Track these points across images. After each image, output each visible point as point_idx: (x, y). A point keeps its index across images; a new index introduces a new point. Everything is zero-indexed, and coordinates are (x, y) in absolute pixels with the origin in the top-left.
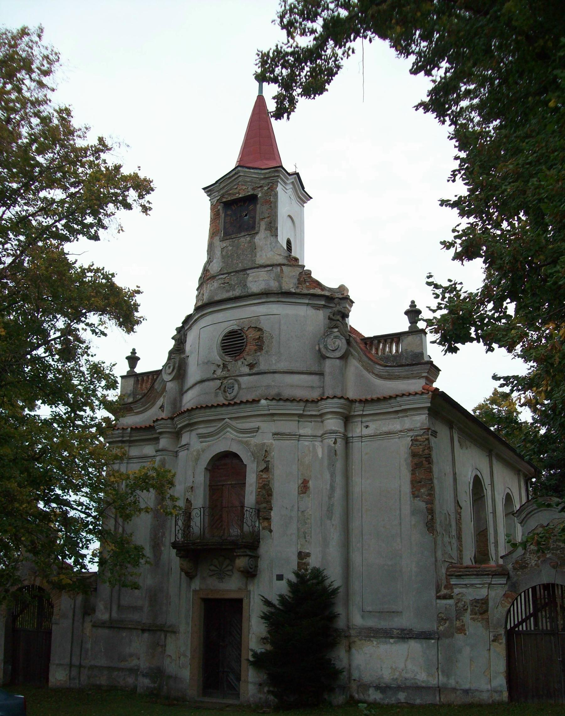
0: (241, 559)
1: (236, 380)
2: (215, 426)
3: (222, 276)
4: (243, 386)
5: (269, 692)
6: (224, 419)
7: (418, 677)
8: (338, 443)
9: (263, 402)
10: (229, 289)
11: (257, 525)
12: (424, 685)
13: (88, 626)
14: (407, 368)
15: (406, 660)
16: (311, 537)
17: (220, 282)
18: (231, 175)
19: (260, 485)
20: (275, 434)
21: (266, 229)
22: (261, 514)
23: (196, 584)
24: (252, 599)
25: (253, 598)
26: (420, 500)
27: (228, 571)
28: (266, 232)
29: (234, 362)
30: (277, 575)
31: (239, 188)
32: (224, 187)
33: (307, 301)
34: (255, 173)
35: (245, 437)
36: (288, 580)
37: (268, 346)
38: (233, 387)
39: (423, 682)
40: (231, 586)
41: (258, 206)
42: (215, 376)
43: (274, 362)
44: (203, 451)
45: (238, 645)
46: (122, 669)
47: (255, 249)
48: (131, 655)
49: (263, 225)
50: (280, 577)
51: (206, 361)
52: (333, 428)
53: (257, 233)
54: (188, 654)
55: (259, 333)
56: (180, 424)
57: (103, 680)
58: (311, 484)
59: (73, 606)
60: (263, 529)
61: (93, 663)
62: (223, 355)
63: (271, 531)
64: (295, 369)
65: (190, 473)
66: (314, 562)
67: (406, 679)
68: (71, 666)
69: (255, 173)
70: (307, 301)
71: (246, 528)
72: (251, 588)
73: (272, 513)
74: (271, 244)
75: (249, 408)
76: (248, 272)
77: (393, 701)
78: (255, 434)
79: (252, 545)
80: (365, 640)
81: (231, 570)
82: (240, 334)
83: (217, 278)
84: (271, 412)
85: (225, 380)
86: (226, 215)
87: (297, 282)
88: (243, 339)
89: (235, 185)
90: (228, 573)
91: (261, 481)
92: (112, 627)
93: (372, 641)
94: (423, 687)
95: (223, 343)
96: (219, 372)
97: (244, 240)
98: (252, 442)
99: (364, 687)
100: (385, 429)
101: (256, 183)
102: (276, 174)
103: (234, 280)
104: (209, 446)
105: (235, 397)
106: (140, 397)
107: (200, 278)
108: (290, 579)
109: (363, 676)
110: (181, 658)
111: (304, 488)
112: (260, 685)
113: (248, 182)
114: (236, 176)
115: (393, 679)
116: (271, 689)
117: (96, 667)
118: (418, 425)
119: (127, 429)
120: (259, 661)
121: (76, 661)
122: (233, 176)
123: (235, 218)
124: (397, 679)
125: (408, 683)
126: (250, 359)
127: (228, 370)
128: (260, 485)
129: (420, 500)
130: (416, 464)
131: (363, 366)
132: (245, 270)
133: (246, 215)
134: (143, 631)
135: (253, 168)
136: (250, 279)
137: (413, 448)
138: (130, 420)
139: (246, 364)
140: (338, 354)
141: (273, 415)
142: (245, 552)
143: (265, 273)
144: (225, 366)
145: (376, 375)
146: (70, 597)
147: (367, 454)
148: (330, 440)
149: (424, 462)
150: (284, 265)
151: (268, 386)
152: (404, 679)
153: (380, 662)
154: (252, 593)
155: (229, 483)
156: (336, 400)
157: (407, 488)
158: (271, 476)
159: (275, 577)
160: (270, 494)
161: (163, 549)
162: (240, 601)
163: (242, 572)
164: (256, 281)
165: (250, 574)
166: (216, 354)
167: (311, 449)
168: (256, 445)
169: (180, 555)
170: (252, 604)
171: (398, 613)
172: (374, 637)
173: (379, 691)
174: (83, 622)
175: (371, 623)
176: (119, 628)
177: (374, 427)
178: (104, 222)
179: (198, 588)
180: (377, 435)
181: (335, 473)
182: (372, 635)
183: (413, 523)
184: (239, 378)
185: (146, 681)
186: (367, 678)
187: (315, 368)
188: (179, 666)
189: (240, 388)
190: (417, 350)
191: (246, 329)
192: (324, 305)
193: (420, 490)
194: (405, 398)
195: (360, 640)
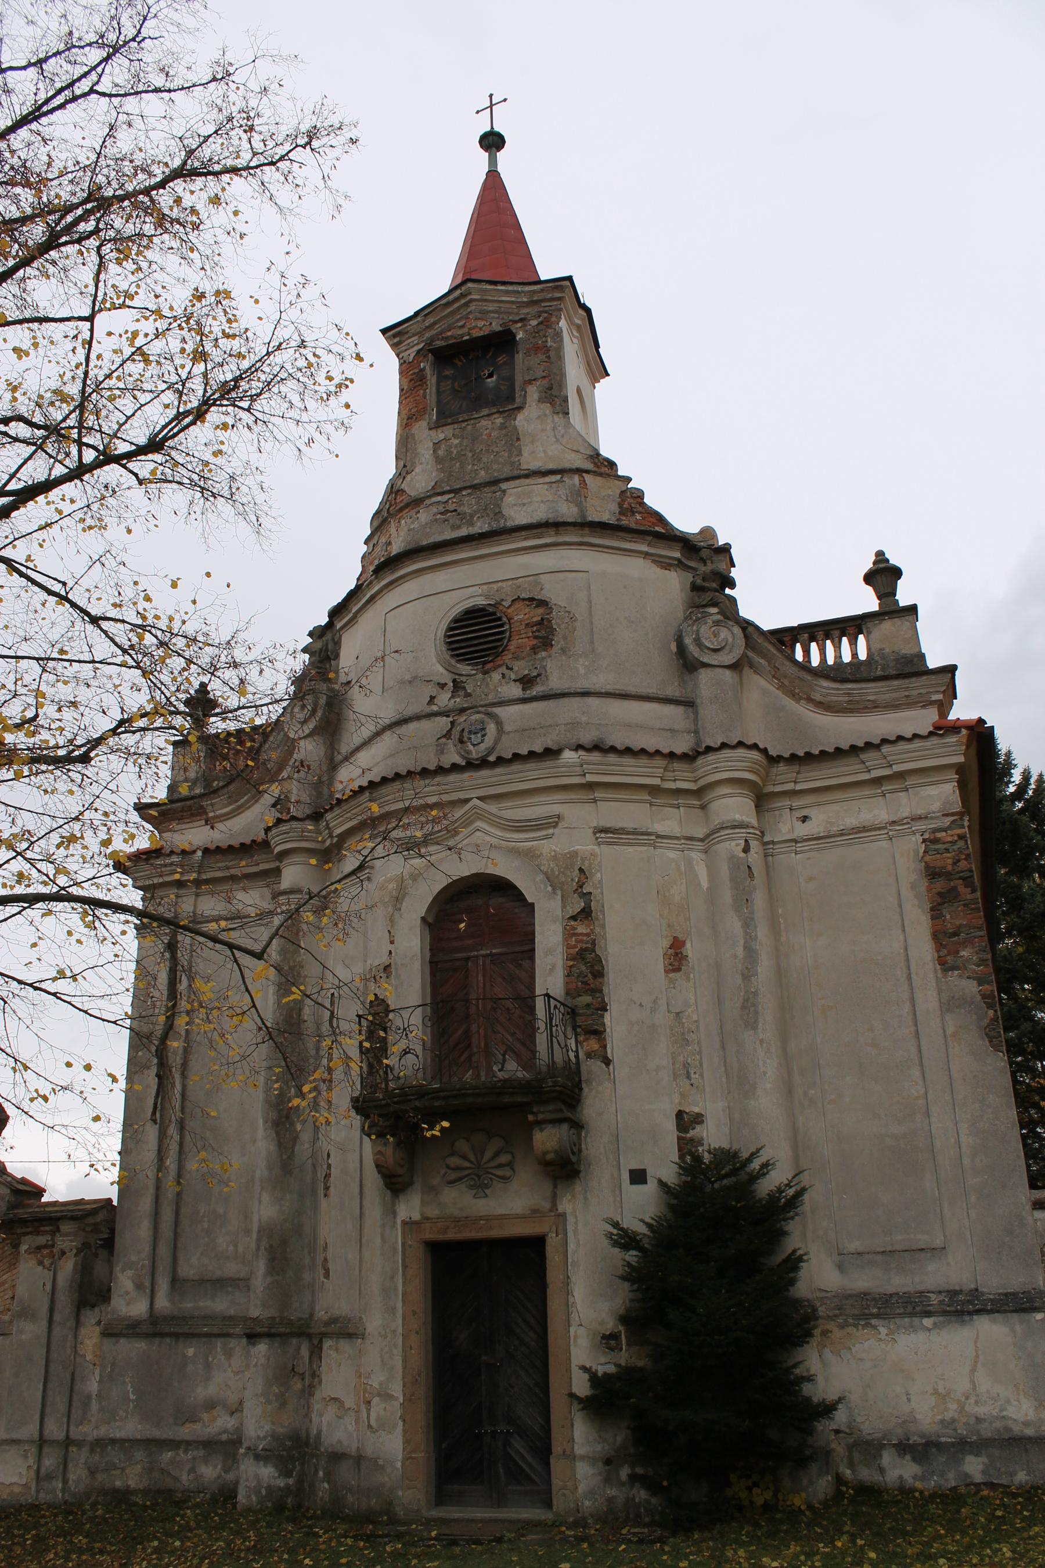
0: (546, 1133)
1: (489, 714)
3: (439, 498)
4: (508, 728)
5: (633, 1478)
6: (467, 801)
7: (1011, 1412)
8: (752, 851)
9: (568, 755)
10: (458, 522)
12: (1029, 1432)
13: (90, 1337)
14: (896, 683)
15: (973, 1371)
16: (702, 1075)
17: (435, 510)
18: (451, 298)
19: (571, 951)
20: (601, 831)
21: (540, 400)
22: (580, 1021)
23: (410, 1208)
24: (570, 1234)
25: (576, 1230)
26: (960, 976)
27: (500, 1166)
28: (542, 406)
29: (480, 676)
30: (631, 1172)
31: (468, 325)
32: (435, 323)
33: (645, 548)
34: (507, 292)
35: (523, 840)
36: (660, 1181)
37: (565, 638)
38: (483, 729)
39: (1026, 1424)
40: (509, 1205)
41: (519, 357)
42: (435, 708)
43: (582, 671)
44: (414, 877)
45: (539, 1358)
46: (188, 1444)
47: (518, 439)
48: (211, 1405)
49: (533, 393)
50: (638, 1177)
51: (408, 677)
52: (738, 817)
53: (520, 408)
54: (397, 1390)
55: (540, 611)
56: (341, 824)
57: (132, 1477)
58: (689, 949)
59: (49, 1287)
60: (589, 1056)
61: (103, 1432)
62: (453, 662)
63: (607, 1062)
64: (632, 690)
66: (713, 1135)
67: (979, 1420)
68: (42, 1442)
69: (507, 292)
70: (645, 548)
72: (565, 1205)
73: (607, 1019)
74: (554, 429)
75: (532, 775)
76: (504, 486)
77: (951, 1480)
78: (551, 831)
79: (561, 1095)
80: (856, 1326)
82: (494, 614)
83: (428, 502)
84: (589, 778)
85: (462, 716)
86: (441, 379)
87: (617, 510)
88: (502, 626)
89: (458, 321)
90: (500, 1172)
91: (573, 941)
92: (154, 1335)
93: (875, 1327)
94: (1029, 1439)
95: (450, 636)
96: (444, 699)
97: (489, 425)
98: (545, 851)
99: (868, 1448)
100: (851, 821)
101: (510, 313)
102: (557, 295)
103: (469, 503)
105: (491, 751)
106: (221, 784)
107: (378, 513)
108: (664, 1180)
109: (859, 1419)
110: (371, 1403)
111: (676, 957)
112: (608, 1462)
113: (491, 312)
114: (463, 301)
115: (942, 1421)
116: (639, 1470)
117: (113, 1441)
118: (936, 806)
119: (194, 852)
120: (605, 1399)
121: (54, 1430)
122: (457, 300)
123: (463, 383)
124: (953, 1421)
125: (986, 1431)
126: (522, 668)
128: (571, 951)
129: (960, 976)
130: (939, 894)
131: (781, 687)
132: (496, 482)
133: (491, 376)
134: (252, 1337)
135: (504, 283)
136: (509, 500)
137: (927, 858)
138: (194, 836)
139: (513, 677)
140: (728, 659)
141: (591, 786)
142: (561, 1110)
143: (546, 486)
144: (458, 686)
145: (819, 704)
146: (41, 1263)
147: (811, 879)
148: (733, 843)
149: (961, 889)
150: (587, 472)
151: (574, 725)
152: (972, 1421)
153: (897, 1381)
154: (570, 1220)
155: (483, 952)
156: (741, 752)
157: (924, 950)
158: (597, 930)
159: (626, 1177)
160: (599, 973)
161: (299, 1127)
162: (538, 1243)
164: (524, 505)
165: (565, 1169)
166: (434, 660)
167: (683, 868)
168: (555, 858)
170: (571, 1246)
171: (936, 1252)
172: (878, 1316)
173: (908, 1457)
174: (78, 1324)
175: (864, 1280)
176: (176, 1336)
177: (823, 818)
179: (416, 1216)
180: (834, 836)
181: (752, 919)
182: (875, 1311)
183: (950, 1030)
184: (497, 710)
185: (267, 1473)
186: (870, 1426)
187: (672, 690)
188: (370, 1426)
190: (915, 651)
191: (506, 604)
192: (679, 560)
193: (958, 952)
194: (902, 746)
195: (841, 1327)
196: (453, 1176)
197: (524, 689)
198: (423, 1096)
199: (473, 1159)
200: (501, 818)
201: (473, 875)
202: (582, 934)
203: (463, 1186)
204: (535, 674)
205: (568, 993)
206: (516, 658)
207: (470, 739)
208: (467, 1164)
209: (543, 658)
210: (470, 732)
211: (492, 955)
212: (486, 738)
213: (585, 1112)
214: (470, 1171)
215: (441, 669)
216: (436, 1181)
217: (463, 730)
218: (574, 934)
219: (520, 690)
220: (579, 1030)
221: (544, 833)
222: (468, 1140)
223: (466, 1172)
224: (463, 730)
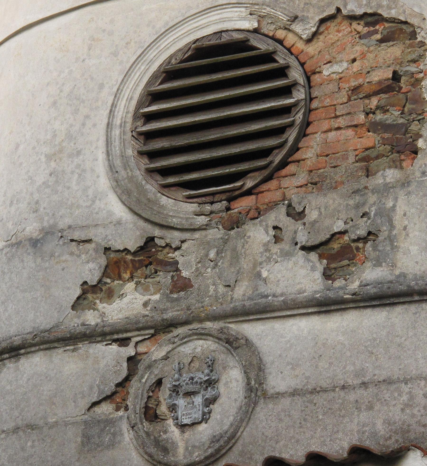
1: (232, 343)
4: (278, 381)
29: (216, 234)
38: (210, 383)
55: (394, 51)
62: (151, 188)
82: (269, 57)
88: (286, 91)
126: (329, 212)
127: (182, 285)
139: (303, 238)
166: (104, 182)
184: (252, 330)
189: (256, 391)
197: (327, 275)
204: (362, 232)
206: (315, 184)
207: (173, 408)
209: (387, 188)
210: (175, 390)
212: (216, 408)
215: (119, 211)
217: (159, 383)
219: (318, 275)
224: (159, 383)
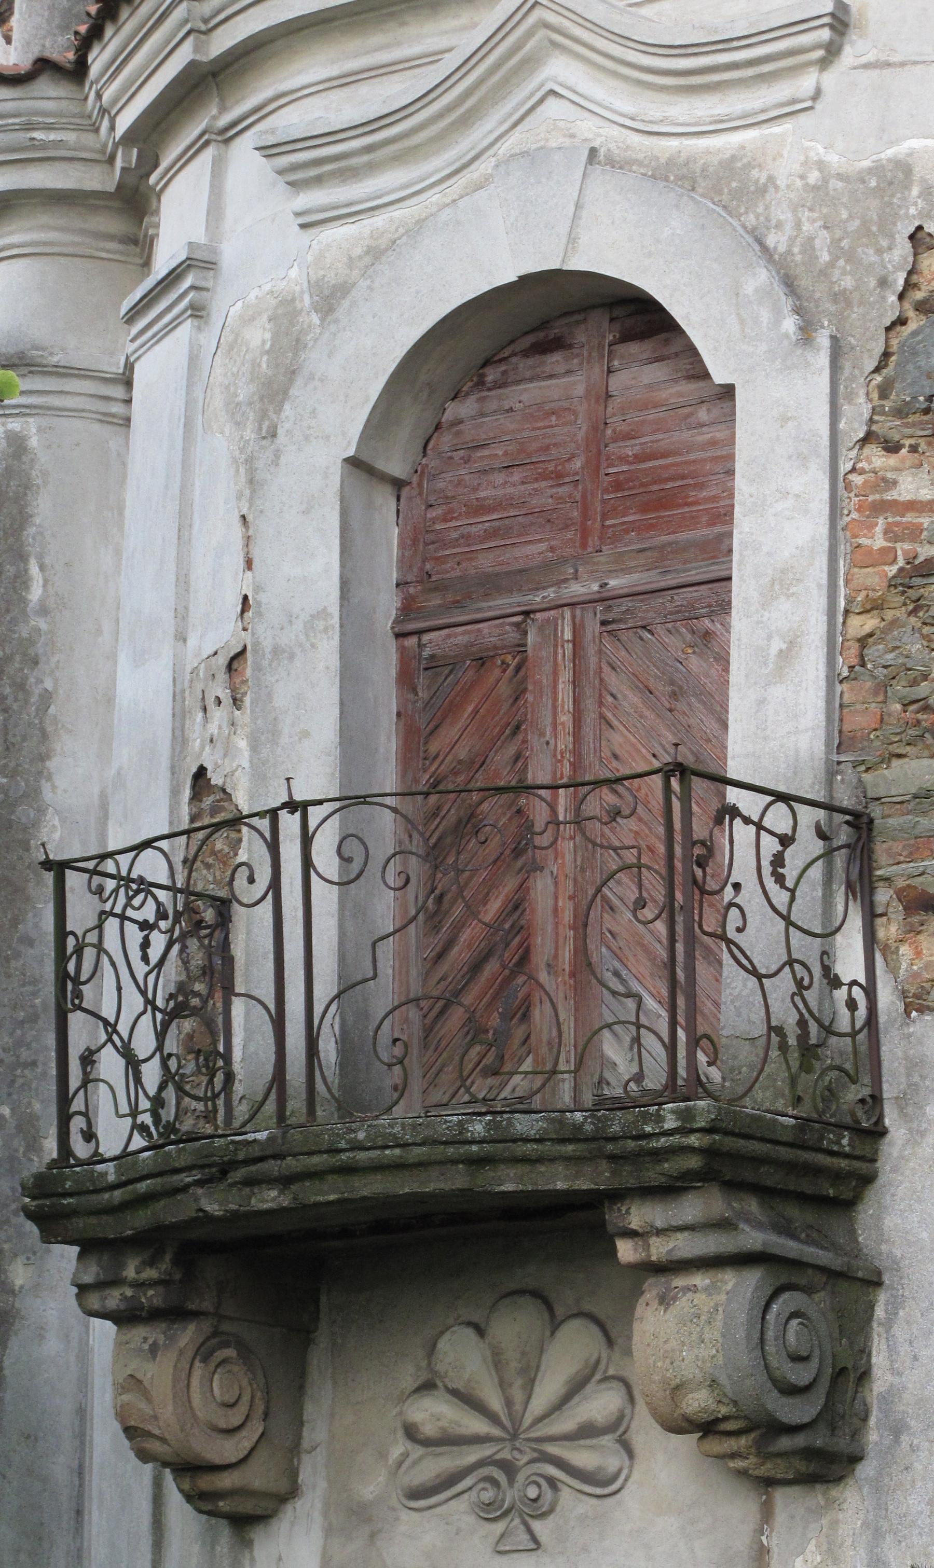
2: (432, 58)
11: (850, 963)
27: (587, 1431)
44: (330, 299)
65: (217, 532)
71: (739, 1005)
78: (806, 83)
81: (617, 1429)
98: (786, 169)
104: (376, 253)
155: (577, 589)
163: (707, 1428)
169: (114, 1299)
178: (901, 499)
196: (431, 1467)
198: (225, 1170)
199: (496, 1404)
200: (624, 39)
201: (526, 281)
202: (912, 506)
203: (460, 1505)
205: (842, 740)
208: (476, 1425)
211: (605, 599)
213: (889, 1222)
214: (487, 1451)
216: (372, 1486)
218: (881, 507)
220: (883, 896)
221: (780, 91)
222: (480, 1331)
223: (473, 1455)
